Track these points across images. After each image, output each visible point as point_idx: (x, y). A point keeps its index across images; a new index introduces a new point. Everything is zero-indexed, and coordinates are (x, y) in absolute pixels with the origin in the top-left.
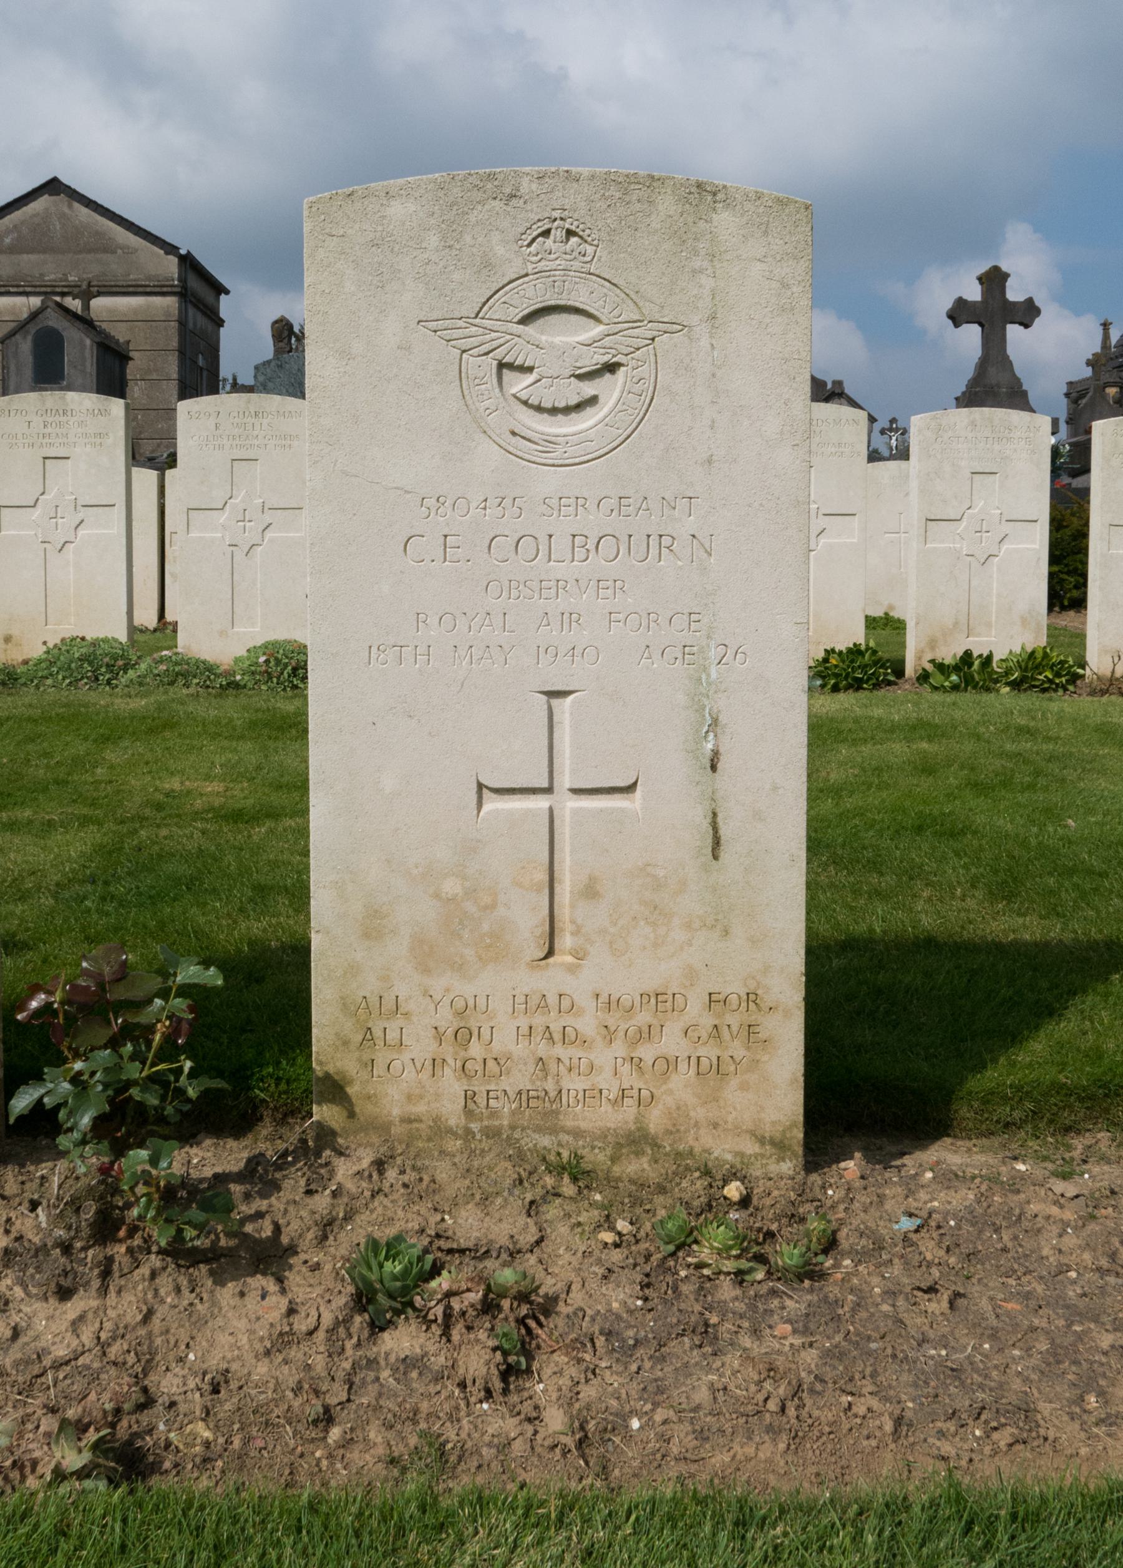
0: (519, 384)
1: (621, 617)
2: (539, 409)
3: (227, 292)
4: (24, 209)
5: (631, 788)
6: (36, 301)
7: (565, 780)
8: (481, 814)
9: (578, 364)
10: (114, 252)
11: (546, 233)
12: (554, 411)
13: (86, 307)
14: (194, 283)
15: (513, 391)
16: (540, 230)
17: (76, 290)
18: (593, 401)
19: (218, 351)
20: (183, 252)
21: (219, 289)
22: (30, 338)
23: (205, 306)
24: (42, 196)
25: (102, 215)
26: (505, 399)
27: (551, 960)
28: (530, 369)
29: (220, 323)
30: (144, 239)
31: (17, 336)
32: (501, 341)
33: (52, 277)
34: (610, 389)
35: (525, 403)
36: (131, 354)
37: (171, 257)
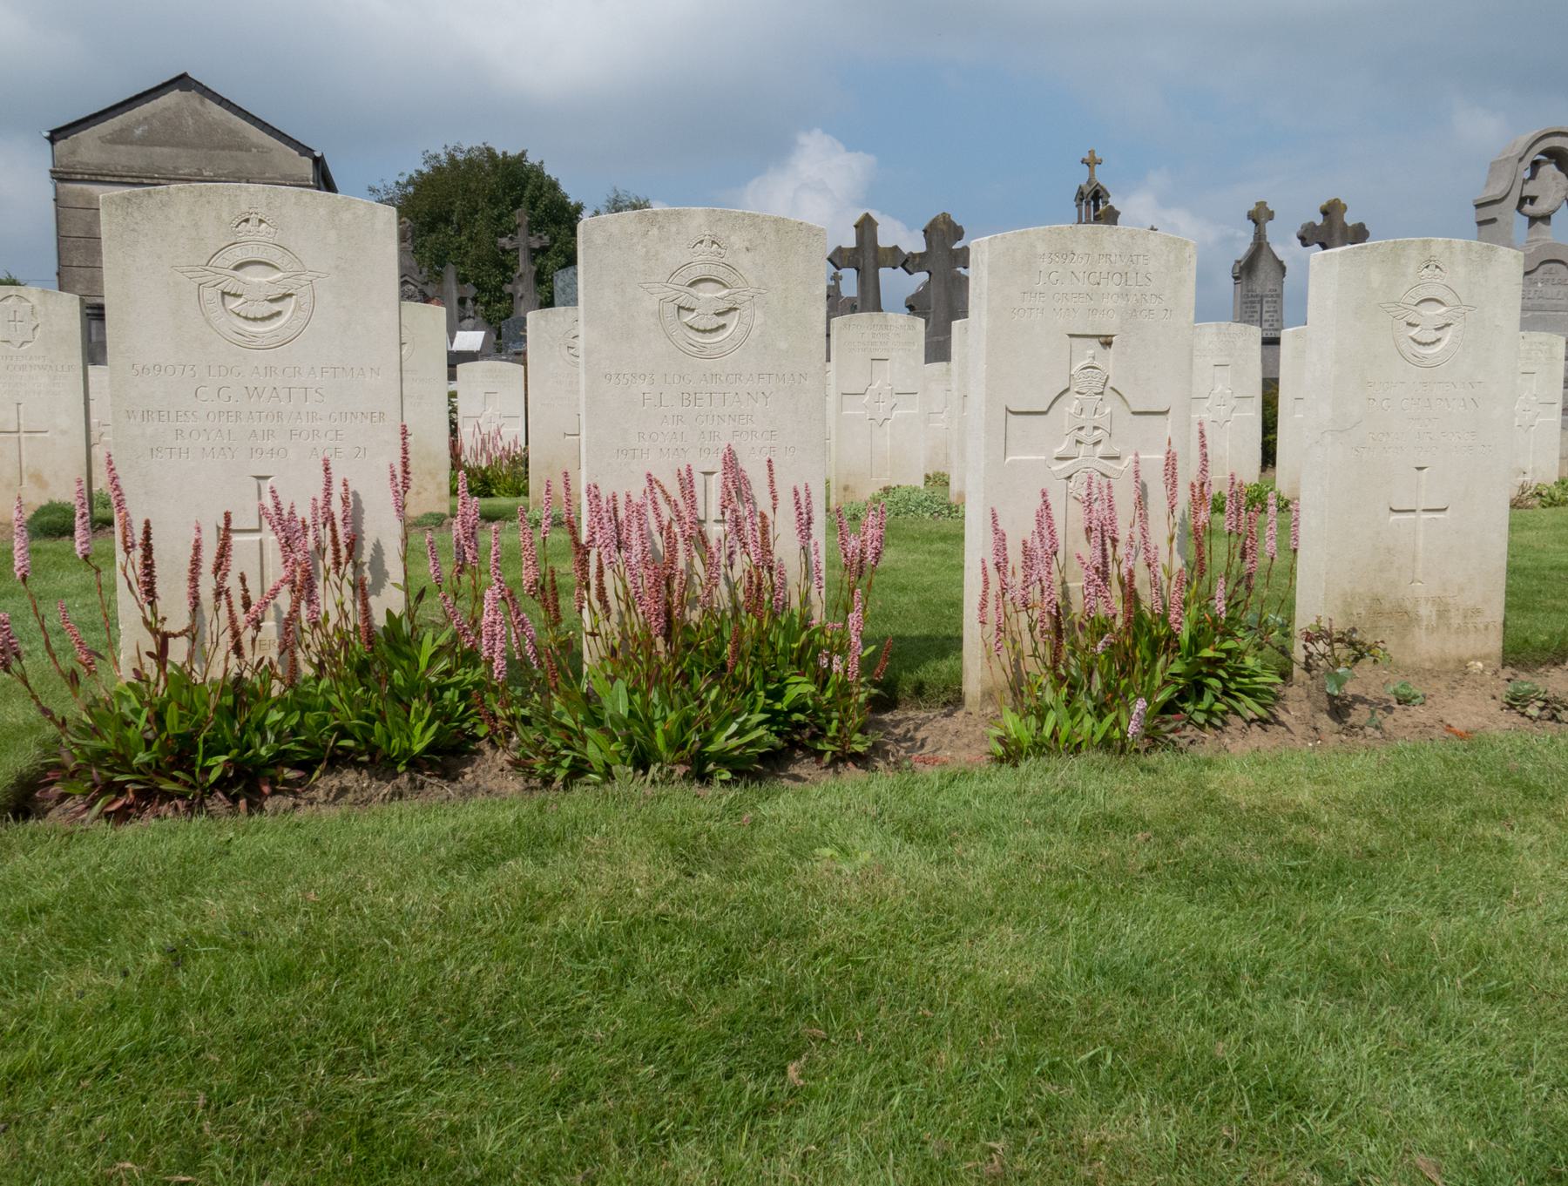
0: (233, 304)
11: (247, 220)
18: (279, 313)
20: (318, 154)
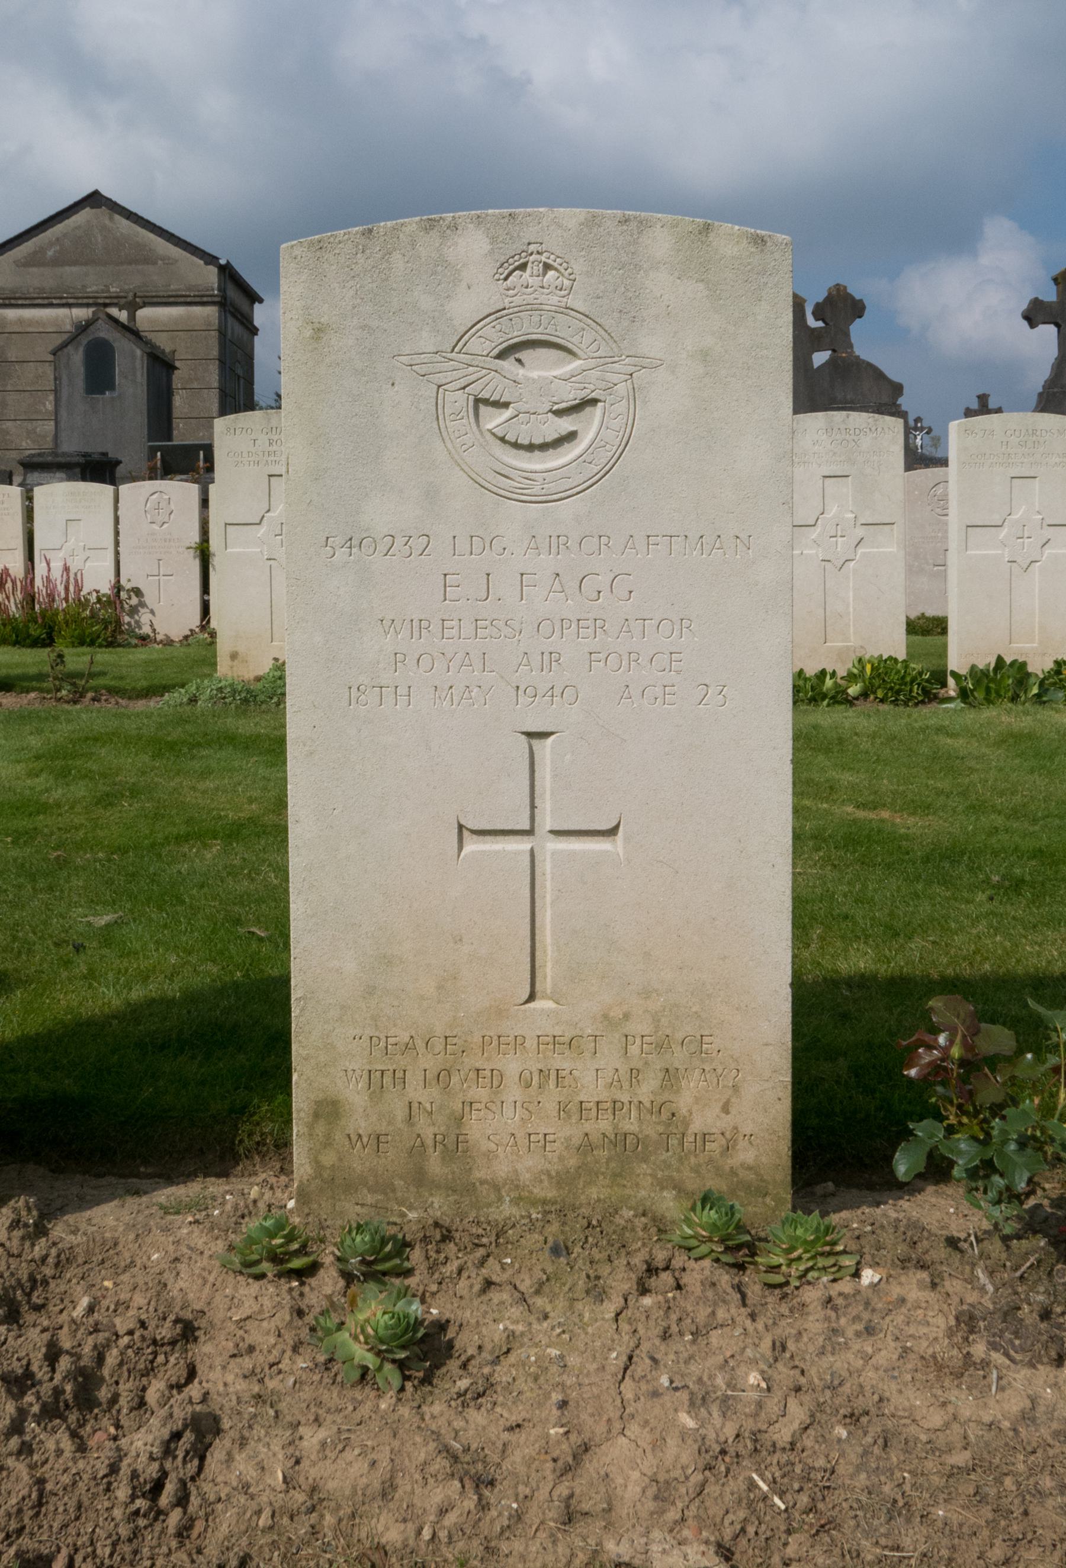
0: (493, 420)
1: (602, 656)
2: (516, 445)
3: (261, 301)
4: (67, 221)
5: (613, 832)
6: (91, 310)
7: (547, 821)
8: (463, 854)
9: (555, 399)
10: (155, 263)
12: (531, 448)
13: (132, 317)
14: (233, 293)
15: (490, 426)
16: (517, 264)
17: (123, 301)
18: (571, 436)
19: (252, 359)
20: (223, 262)
21: (254, 298)
22: (81, 349)
23: (242, 315)
24: (83, 208)
25: (143, 227)
26: (482, 433)
27: (531, 1005)
28: (506, 405)
29: (254, 331)
30: (185, 250)
31: (69, 347)
32: (480, 374)
33: (94, 288)
34: (589, 426)
35: (502, 439)
36: (177, 364)
37: (211, 267)
